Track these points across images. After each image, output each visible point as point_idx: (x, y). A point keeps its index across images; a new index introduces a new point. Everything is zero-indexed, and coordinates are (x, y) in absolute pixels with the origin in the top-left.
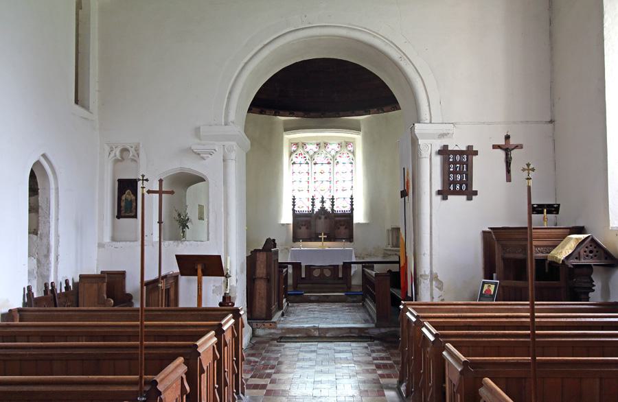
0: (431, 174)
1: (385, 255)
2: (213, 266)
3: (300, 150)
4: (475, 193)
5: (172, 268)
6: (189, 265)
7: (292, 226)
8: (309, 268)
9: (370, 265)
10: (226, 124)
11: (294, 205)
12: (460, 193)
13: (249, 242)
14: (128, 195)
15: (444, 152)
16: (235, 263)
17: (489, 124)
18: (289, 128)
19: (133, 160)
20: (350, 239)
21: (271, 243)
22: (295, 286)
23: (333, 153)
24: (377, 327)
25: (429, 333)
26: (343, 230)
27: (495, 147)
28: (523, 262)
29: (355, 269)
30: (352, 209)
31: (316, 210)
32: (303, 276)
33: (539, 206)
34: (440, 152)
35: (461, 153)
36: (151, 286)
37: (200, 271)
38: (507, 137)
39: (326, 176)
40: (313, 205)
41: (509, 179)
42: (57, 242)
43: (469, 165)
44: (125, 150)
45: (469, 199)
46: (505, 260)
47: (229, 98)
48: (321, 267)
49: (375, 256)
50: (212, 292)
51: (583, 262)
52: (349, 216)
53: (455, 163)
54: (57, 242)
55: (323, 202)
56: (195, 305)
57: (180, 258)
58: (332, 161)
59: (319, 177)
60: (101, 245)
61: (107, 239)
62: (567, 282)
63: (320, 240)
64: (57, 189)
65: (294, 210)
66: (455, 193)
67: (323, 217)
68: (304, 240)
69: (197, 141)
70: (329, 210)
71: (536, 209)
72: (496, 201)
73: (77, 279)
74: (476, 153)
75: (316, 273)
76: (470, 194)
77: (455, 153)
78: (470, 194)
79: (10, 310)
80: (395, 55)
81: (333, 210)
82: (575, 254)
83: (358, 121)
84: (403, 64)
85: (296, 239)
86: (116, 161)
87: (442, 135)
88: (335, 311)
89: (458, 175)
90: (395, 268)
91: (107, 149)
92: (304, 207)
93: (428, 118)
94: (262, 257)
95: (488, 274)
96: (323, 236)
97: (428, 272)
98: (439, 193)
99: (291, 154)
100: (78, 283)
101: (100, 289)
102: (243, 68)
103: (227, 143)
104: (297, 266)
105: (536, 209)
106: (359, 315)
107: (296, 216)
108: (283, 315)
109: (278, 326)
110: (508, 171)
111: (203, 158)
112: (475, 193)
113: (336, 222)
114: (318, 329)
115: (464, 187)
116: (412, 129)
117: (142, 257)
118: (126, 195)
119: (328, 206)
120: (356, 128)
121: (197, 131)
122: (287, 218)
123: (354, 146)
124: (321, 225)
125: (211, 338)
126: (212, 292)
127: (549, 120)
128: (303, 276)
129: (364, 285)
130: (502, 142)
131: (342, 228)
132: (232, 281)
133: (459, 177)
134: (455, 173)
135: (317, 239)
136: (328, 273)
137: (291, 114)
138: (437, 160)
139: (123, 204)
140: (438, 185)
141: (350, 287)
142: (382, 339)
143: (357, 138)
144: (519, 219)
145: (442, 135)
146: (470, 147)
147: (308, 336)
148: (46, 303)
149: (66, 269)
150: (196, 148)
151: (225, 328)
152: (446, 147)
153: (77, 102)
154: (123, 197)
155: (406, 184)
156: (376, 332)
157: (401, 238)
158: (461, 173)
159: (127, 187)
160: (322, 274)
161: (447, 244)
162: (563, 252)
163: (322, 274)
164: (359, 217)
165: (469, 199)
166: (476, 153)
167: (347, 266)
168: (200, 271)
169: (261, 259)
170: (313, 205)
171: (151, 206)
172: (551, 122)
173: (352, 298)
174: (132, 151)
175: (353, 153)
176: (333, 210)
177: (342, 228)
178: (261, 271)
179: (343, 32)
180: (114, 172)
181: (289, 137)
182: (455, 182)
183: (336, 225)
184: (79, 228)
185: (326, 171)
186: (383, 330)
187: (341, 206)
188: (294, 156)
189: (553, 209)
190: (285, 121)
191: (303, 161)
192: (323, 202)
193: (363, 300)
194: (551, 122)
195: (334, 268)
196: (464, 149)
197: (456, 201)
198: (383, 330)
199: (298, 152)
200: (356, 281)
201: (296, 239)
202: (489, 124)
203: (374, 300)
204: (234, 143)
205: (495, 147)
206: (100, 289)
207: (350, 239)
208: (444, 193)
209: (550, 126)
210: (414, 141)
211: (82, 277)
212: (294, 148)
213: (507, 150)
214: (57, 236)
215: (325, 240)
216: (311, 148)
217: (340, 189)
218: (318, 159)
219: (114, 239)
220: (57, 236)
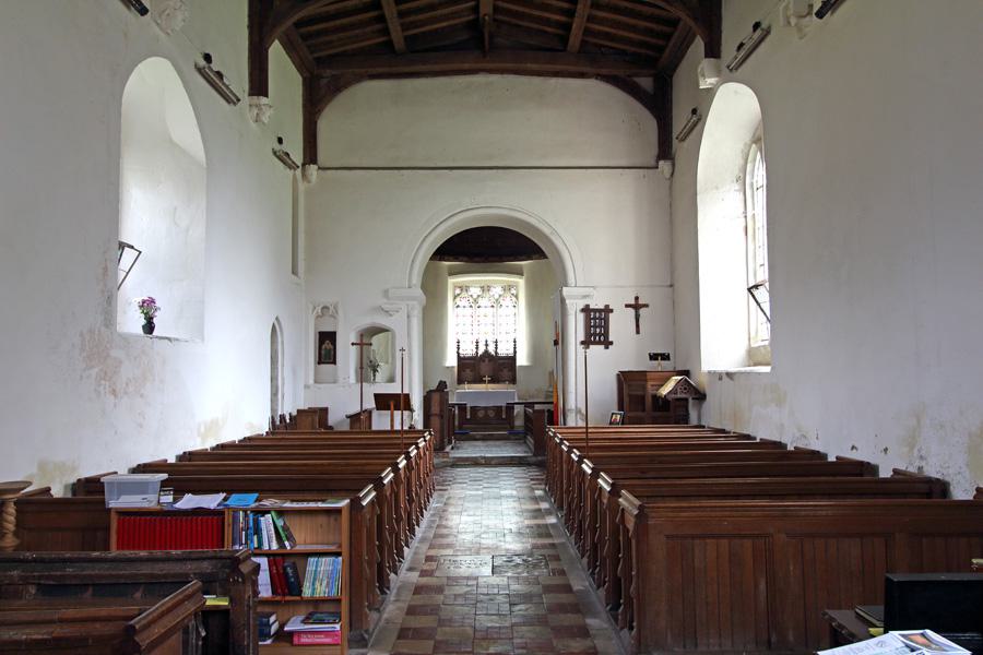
0: (576, 328)
1: (547, 397)
2: (400, 402)
3: (464, 294)
4: (611, 343)
5: (370, 404)
6: (383, 401)
7: (456, 370)
8: (474, 409)
9: (530, 405)
10: (410, 287)
11: (458, 349)
12: (599, 343)
13: (425, 384)
14: (327, 345)
15: (586, 310)
16: (417, 402)
17: (621, 287)
18: (453, 273)
19: (332, 316)
20: (513, 381)
21: (442, 385)
22: (460, 427)
23: (497, 296)
24: (535, 455)
25: (587, 467)
26: (506, 373)
27: (627, 306)
28: (643, 398)
29: (518, 409)
30: (515, 352)
31: (480, 353)
32: (468, 417)
33: (655, 354)
34: (583, 310)
35: (600, 311)
36: (354, 418)
37: (392, 407)
38: (637, 298)
39: (490, 320)
40: (477, 348)
41: (638, 332)
42: (283, 384)
43: (607, 320)
44: (325, 308)
45: (607, 348)
46: (630, 396)
47: (412, 265)
48: (486, 408)
49: (538, 397)
50: (399, 421)
51: (679, 396)
52: (513, 359)
53: (595, 318)
54: (283, 384)
55: (487, 345)
56: (389, 428)
57: (376, 396)
58: (497, 304)
59: (482, 319)
60: (307, 387)
61: (311, 381)
62: (672, 410)
63: (484, 382)
64: (283, 342)
65: (458, 353)
66: (595, 343)
67: (487, 360)
68: (469, 383)
69: (385, 301)
70: (493, 353)
71: (653, 357)
72: (627, 350)
73: (294, 413)
74: (612, 311)
75: (481, 414)
76: (608, 344)
77: (595, 311)
78: (608, 344)
79: (185, 453)
80: (546, 231)
81: (496, 353)
82: (674, 391)
83: (521, 266)
84: (553, 238)
85: (460, 381)
86: (318, 317)
87: (585, 297)
88: (499, 446)
89: (597, 328)
90: (551, 407)
91: (311, 307)
92: (468, 350)
93: (573, 280)
94: (436, 397)
95: (621, 407)
96: (487, 379)
97: (573, 407)
98: (582, 343)
99: (455, 298)
100: (295, 417)
101: (313, 420)
102: (424, 240)
103: (410, 303)
104: (462, 407)
105: (653, 357)
106: (524, 448)
107: (461, 359)
108: (452, 448)
109: (450, 455)
110: (638, 326)
111: (391, 315)
112: (611, 343)
113: (500, 365)
114: (485, 458)
115: (602, 338)
116: (561, 291)
117: (343, 397)
118: (326, 347)
119: (491, 349)
120: (519, 273)
121: (386, 293)
122: (451, 361)
123: (517, 289)
124: (485, 368)
125: (369, 492)
126: (399, 421)
127: (669, 283)
128: (468, 417)
129: (526, 426)
130: (633, 302)
131: (505, 371)
132: (415, 415)
133: (598, 330)
134: (595, 327)
135: (483, 382)
136: (492, 414)
137: (456, 259)
138: (581, 316)
139: (323, 352)
140: (581, 337)
141: (513, 427)
142: (540, 465)
143: (521, 282)
144: (646, 365)
145: (585, 297)
146: (607, 306)
147: (475, 463)
148: (280, 425)
149: (288, 408)
150: (386, 307)
151: (385, 482)
152: (588, 306)
153: (293, 273)
154: (324, 347)
155: (557, 335)
156: (534, 459)
157: (556, 379)
158: (600, 327)
159: (327, 340)
160: (486, 415)
161: (590, 384)
162: (665, 390)
163: (486, 415)
164: (522, 360)
165: (607, 348)
166: (612, 311)
167: (510, 407)
168: (392, 407)
169: (436, 395)
170: (477, 348)
171: (347, 354)
172: (671, 286)
173: (513, 436)
174: (332, 308)
175: (516, 297)
176: (496, 353)
177: (505, 371)
178: (435, 409)
179: (505, 212)
180: (316, 328)
181: (452, 281)
182: (595, 334)
183: (495, 367)
184: (294, 372)
185: (489, 316)
186: (539, 458)
187: (505, 350)
188: (458, 299)
189: (665, 357)
190: (450, 267)
191: (467, 304)
192: (487, 345)
193: (525, 437)
194: (671, 286)
195: (498, 409)
196: (602, 307)
197: (596, 349)
198: (539, 458)
199: (462, 295)
200: (519, 422)
201: (460, 381)
202: (621, 287)
203: (532, 435)
204: (415, 303)
205: (627, 306)
206: (313, 420)
207: (513, 381)
208: (586, 343)
209: (670, 289)
210: (563, 301)
211: (298, 411)
212: (458, 291)
213: (636, 306)
214: (283, 379)
215: (490, 382)
216: (475, 291)
217: (504, 332)
218: (481, 302)
219: (316, 382)
220: (283, 379)
